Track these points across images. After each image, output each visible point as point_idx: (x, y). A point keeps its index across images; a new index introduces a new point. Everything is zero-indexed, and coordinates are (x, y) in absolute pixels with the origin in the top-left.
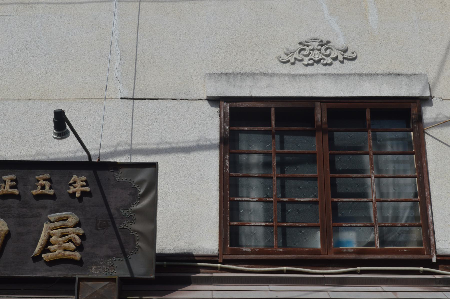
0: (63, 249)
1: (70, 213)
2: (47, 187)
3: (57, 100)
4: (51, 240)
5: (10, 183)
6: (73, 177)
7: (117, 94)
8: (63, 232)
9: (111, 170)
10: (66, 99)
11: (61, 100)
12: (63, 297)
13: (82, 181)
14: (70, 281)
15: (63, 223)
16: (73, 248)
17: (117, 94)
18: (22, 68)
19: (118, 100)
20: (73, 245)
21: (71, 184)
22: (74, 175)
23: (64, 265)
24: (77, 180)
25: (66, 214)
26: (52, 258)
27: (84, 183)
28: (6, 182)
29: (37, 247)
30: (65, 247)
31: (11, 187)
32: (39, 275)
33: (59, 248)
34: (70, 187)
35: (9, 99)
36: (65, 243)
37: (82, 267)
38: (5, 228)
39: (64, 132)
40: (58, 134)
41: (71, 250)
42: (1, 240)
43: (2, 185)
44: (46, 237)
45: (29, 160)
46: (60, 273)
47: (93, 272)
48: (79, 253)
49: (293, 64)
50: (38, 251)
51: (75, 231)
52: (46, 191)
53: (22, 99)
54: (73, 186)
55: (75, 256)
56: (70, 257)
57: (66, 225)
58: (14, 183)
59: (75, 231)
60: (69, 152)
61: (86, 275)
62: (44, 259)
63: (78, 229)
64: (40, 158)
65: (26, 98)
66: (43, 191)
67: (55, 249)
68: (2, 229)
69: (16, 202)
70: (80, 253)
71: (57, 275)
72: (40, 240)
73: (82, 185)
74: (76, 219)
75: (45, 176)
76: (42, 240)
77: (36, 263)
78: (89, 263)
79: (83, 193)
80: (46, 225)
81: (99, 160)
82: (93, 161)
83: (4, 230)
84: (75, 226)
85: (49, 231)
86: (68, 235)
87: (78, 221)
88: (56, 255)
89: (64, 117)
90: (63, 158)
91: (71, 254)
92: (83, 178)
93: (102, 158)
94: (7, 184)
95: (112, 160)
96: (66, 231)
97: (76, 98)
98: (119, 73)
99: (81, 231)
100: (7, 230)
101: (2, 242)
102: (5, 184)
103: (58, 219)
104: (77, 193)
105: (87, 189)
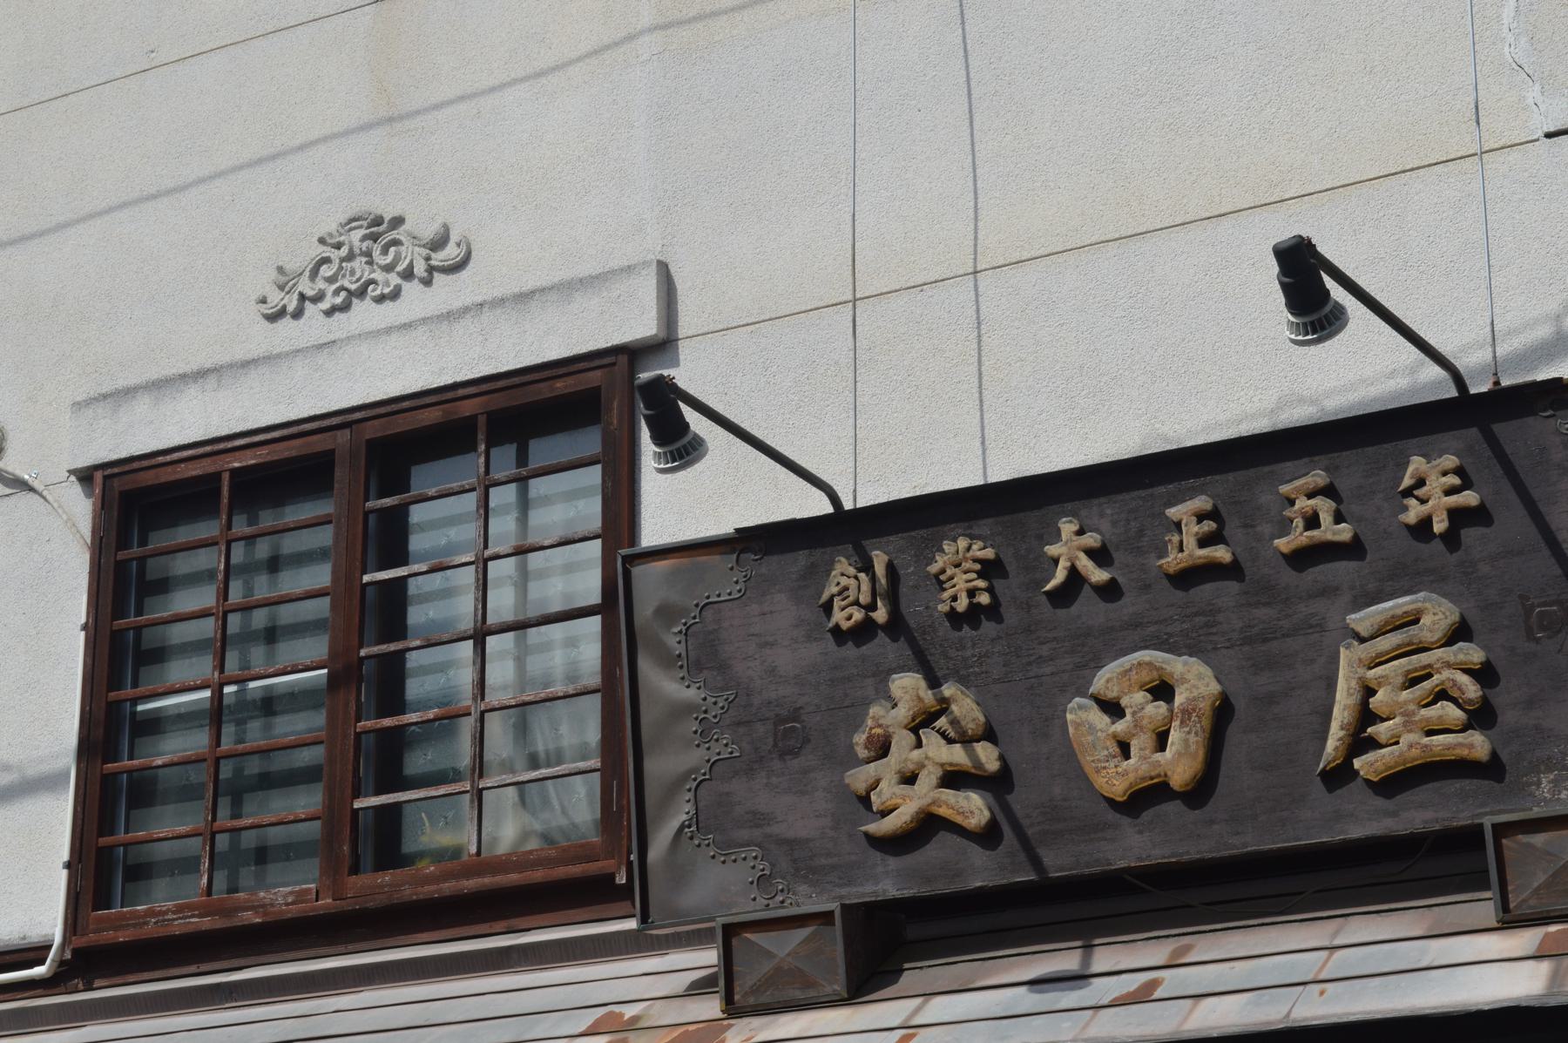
0: (1422, 729)
1: (1422, 594)
2: (1326, 518)
3: (1315, 195)
4: (1375, 702)
5: (1196, 529)
6: (1411, 463)
7: (1528, 124)
8: (1410, 667)
9: (1545, 411)
10: (1348, 185)
11: (1329, 192)
12: (1453, 901)
13: (1445, 474)
14: (1469, 838)
15: (1405, 635)
16: (1454, 719)
17: (1528, 124)
18: (1175, 110)
19: (1537, 143)
20: (1455, 707)
21: (1408, 493)
22: (1411, 458)
23: (1437, 784)
24: (1425, 473)
25: (1410, 604)
26: (1391, 768)
27: (1454, 480)
28: (1183, 526)
29: (1330, 737)
30: (1428, 720)
31: (1204, 542)
32: (1356, 832)
33: (1408, 725)
34: (1406, 501)
35: (1150, 232)
36: (1426, 706)
37: (1503, 785)
38: (1208, 686)
39: (1326, 316)
40: (1305, 325)
41: (1451, 727)
42: (1204, 732)
43: (1170, 540)
44: (1354, 697)
45: (1257, 431)
46: (1429, 814)
47: (1545, 798)
48: (1482, 734)
50: (1336, 749)
51: (1452, 658)
52: (1325, 532)
53: (1195, 221)
54: (1417, 498)
55: (1471, 746)
56: (1453, 755)
57: (1418, 641)
58: (1208, 526)
59: (1452, 659)
60: (1392, 374)
61: (1524, 810)
62: (1362, 773)
63: (1461, 649)
64: (1296, 417)
65: (1208, 215)
66: (1315, 533)
67: (1395, 731)
68: (1200, 691)
69: (1224, 593)
70: (1486, 736)
71: (1418, 827)
72: (1336, 711)
73: (1446, 487)
74: (1448, 614)
75: (1311, 479)
76: (1344, 709)
77: (1339, 792)
78: (1525, 764)
79: (1458, 516)
80: (1348, 652)
81: (1497, 383)
82: (1473, 391)
83: (1208, 693)
84: (1451, 639)
85: (1362, 672)
86: (1429, 676)
87: (1457, 619)
88: (1401, 754)
89: (1315, 261)
90: (1375, 400)
91: (1455, 741)
92: (1447, 462)
93: (1516, 371)
94: (1187, 533)
95: (1543, 375)
96: (1421, 664)
97: (1381, 174)
98: (1522, 42)
99: (1473, 654)
100: (1216, 692)
101: (1207, 736)
102: (1180, 532)
103: (1384, 625)
104: (1435, 519)
105: (1469, 498)
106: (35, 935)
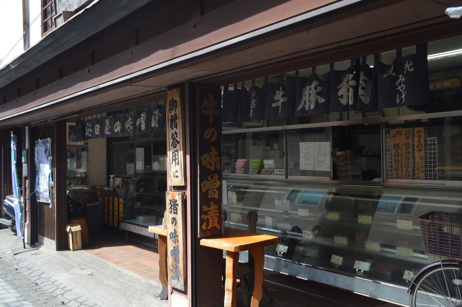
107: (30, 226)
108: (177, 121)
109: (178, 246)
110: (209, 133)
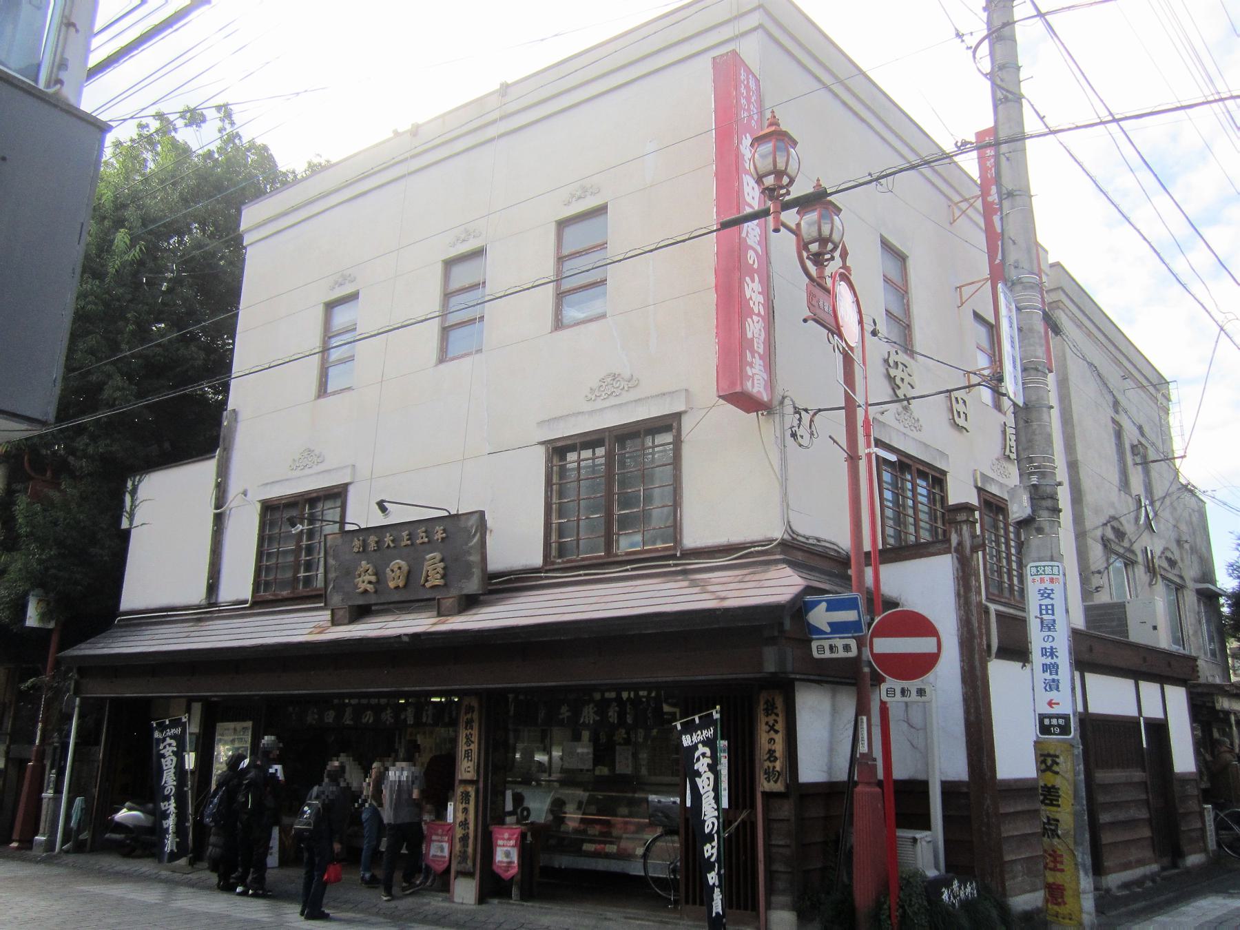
49: (594, 400)
106: (242, 597)
107: (734, 676)
108: (474, 724)
109: (468, 834)
110: (237, 30)
